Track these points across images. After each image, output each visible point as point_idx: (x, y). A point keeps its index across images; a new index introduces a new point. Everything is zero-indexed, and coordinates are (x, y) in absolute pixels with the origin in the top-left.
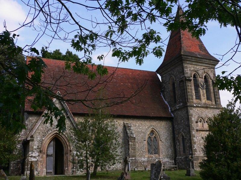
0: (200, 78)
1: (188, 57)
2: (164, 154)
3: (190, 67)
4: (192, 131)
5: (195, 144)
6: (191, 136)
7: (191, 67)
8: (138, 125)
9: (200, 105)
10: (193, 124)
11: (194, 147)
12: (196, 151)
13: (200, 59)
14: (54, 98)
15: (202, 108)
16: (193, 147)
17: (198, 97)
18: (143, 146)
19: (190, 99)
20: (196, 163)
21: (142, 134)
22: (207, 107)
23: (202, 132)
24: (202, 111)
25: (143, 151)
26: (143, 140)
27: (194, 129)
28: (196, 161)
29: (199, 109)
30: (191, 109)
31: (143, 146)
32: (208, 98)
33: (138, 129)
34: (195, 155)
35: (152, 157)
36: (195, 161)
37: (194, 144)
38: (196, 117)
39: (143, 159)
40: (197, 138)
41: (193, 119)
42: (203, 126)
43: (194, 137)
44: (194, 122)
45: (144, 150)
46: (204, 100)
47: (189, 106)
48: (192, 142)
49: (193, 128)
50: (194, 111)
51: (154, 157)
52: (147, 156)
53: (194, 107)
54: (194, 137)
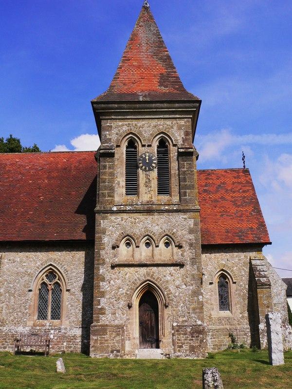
0: (143, 146)
1: (110, 105)
2: (73, 318)
3: (118, 126)
4: (99, 268)
5: (103, 294)
6: (95, 278)
7: (123, 125)
8: (18, 260)
9: (128, 208)
10: (102, 252)
11: (99, 304)
12: (104, 313)
13: (143, 105)
14: (117, 211)
15: (136, 214)
16: (95, 302)
17: (132, 187)
18: (26, 302)
19: (104, 196)
20: (96, 340)
21: (27, 278)
22: (149, 211)
23: (126, 269)
24: (133, 220)
25: (24, 313)
26: (27, 289)
27: (104, 263)
28: (97, 335)
29: (125, 216)
30: (103, 218)
31: (26, 302)
32: (163, 188)
33: (19, 269)
34: (98, 321)
35: (43, 326)
36: (95, 335)
37: (101, 297)
38: (116, 235)
39: (20, 329)
40: (112, 282)
41: (106, 240)
42: (133, 256)
43: (103, 280)
44: (108, 248)
45: (27, 311)
46: (148, 192)
47: (99, 212)
48: (95, 291)
49: (104, 260)
50: (112, 222)
51: (48, 324)
52: (31, 323)
53: (112, 212)
54: (103, 280)
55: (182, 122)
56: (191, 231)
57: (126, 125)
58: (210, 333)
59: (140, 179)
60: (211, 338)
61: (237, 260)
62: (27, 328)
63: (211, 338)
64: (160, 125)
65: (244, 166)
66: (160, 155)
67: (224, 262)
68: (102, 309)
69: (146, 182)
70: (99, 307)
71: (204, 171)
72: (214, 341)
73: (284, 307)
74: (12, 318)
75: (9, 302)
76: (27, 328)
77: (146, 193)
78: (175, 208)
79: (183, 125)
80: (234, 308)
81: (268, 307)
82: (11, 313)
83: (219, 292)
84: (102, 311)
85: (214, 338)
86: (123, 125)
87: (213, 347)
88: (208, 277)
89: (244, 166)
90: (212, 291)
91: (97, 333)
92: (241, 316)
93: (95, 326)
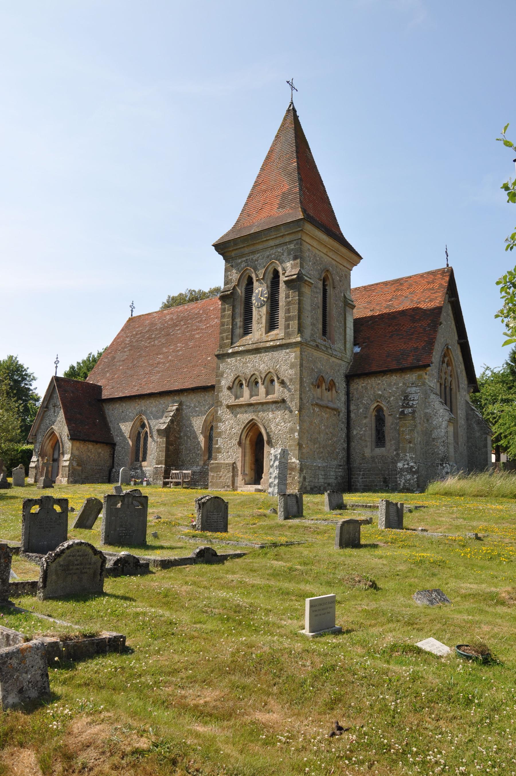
7: (241, 262)
11: (217, 444)
16: (214, 442)
20: (213, 476)
22: (257, 351)
32: (272, 325)
45: (199, 452)
55: (292, 246)
56: (292, 366)
57: (244, 261)
58: (361, 473)
59: (254, 316)
60: (362, 478)
61: (394, 389)
62: (199, 468)
63: (362, 478)
64: (272, 254)
65: (448, 265)
66: (348, 266)
67: (380, 393)
68: (218, 448)
69: (258, 319)
70: (217, 446)
71: (356, 288)
72: (365, 481)
73: (443, 442)
74: (189, 458)
75: (187, 444)
76: (199, 468)
77: (258, 330)
78: (278, 343)
79: (292, 249)
80: (388, 444)
81: (410, 442)
82: (188, 454)
83: (376, 426)
84: (219, 450)
85: (365, 478)
86: (241, 262)
87: (363, 487)
88: (363, 411)
89: (448, 265)
90: (367, 426)
91: (212, 470)
92: (395, 453)
93: (213, 464)
